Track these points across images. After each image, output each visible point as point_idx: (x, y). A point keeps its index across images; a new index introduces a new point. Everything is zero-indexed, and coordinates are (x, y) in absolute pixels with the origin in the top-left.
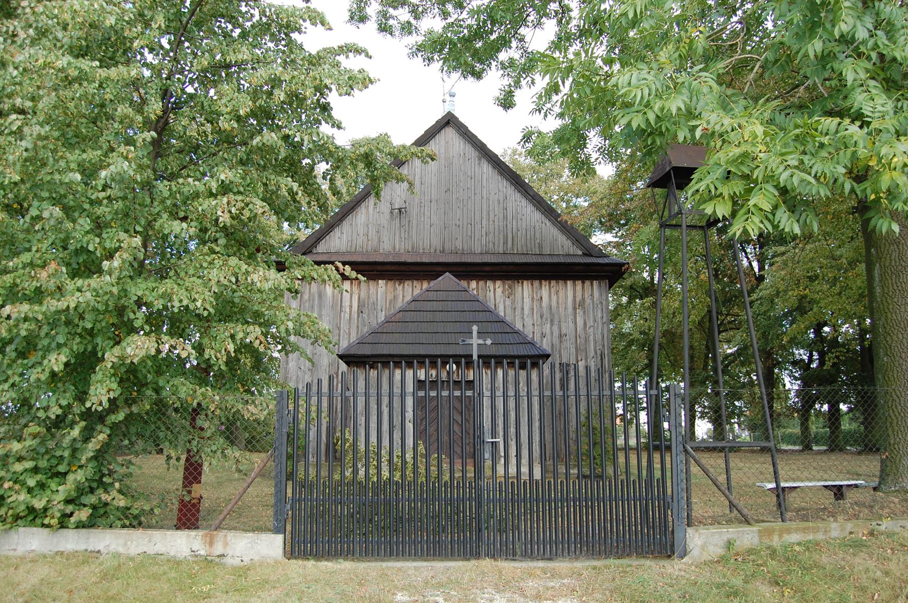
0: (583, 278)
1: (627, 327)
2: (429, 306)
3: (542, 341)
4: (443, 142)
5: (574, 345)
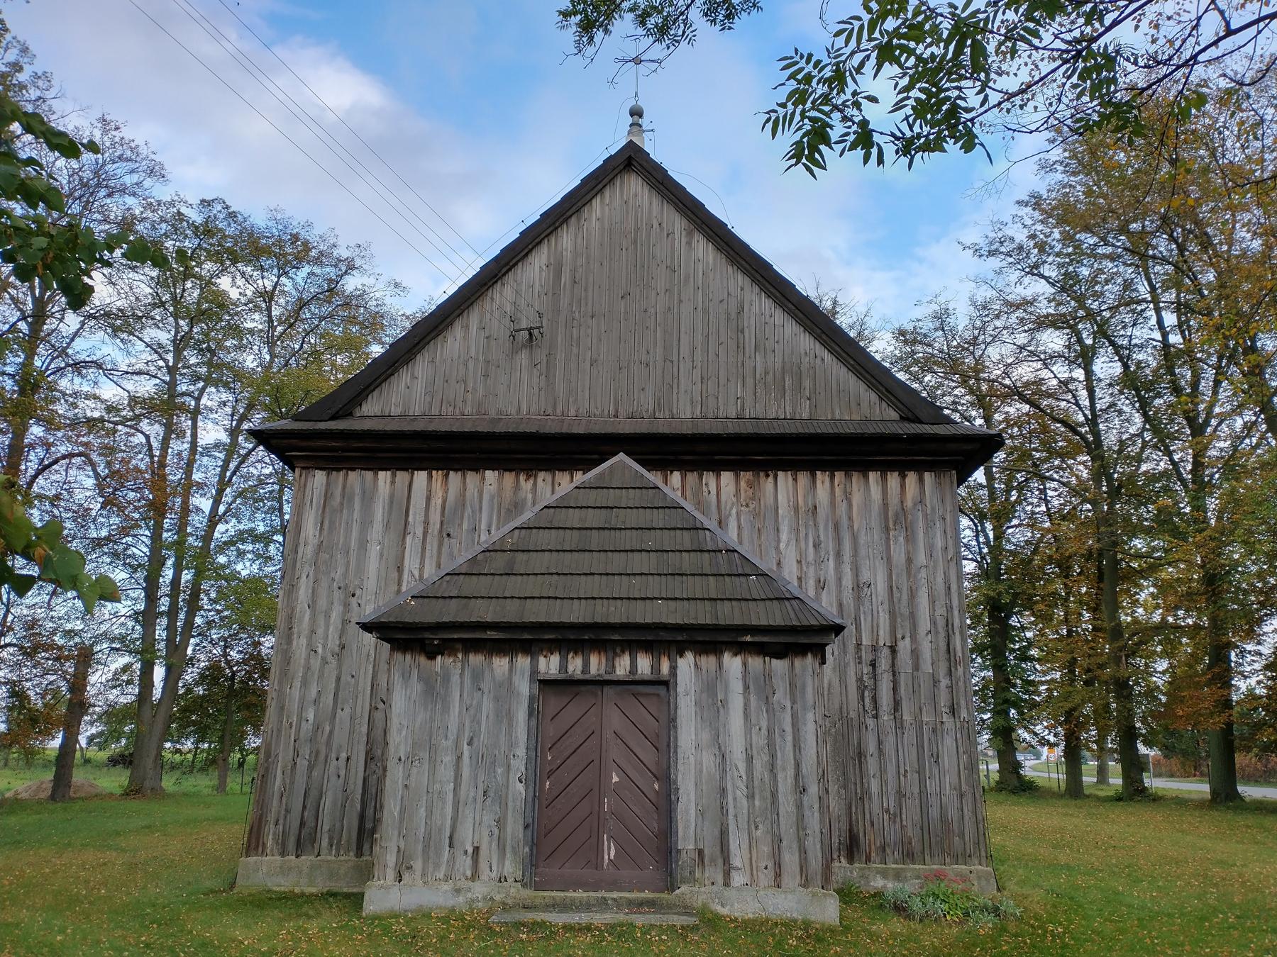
0: (902, 468)
1: (1143, 335)
2: (574, 518)
3: (818, 598)
4: (618, 202)
5: (886, 606)
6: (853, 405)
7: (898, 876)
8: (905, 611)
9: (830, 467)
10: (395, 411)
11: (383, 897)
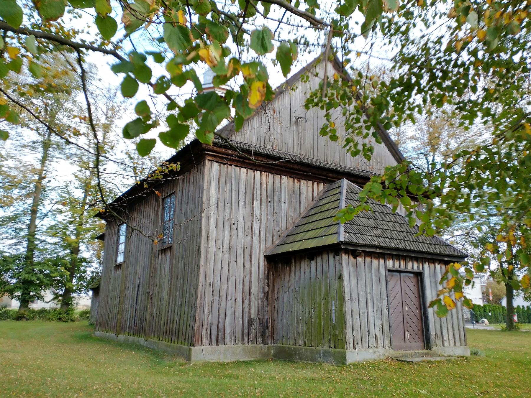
11: (353, 356)
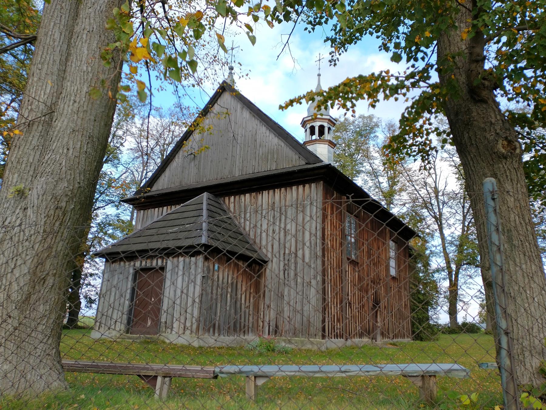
0: (303, 183)
6: (290, 161)
7: (290, 342)
8: (300, 239)
9: (279, 186)
10: (160, 188)
